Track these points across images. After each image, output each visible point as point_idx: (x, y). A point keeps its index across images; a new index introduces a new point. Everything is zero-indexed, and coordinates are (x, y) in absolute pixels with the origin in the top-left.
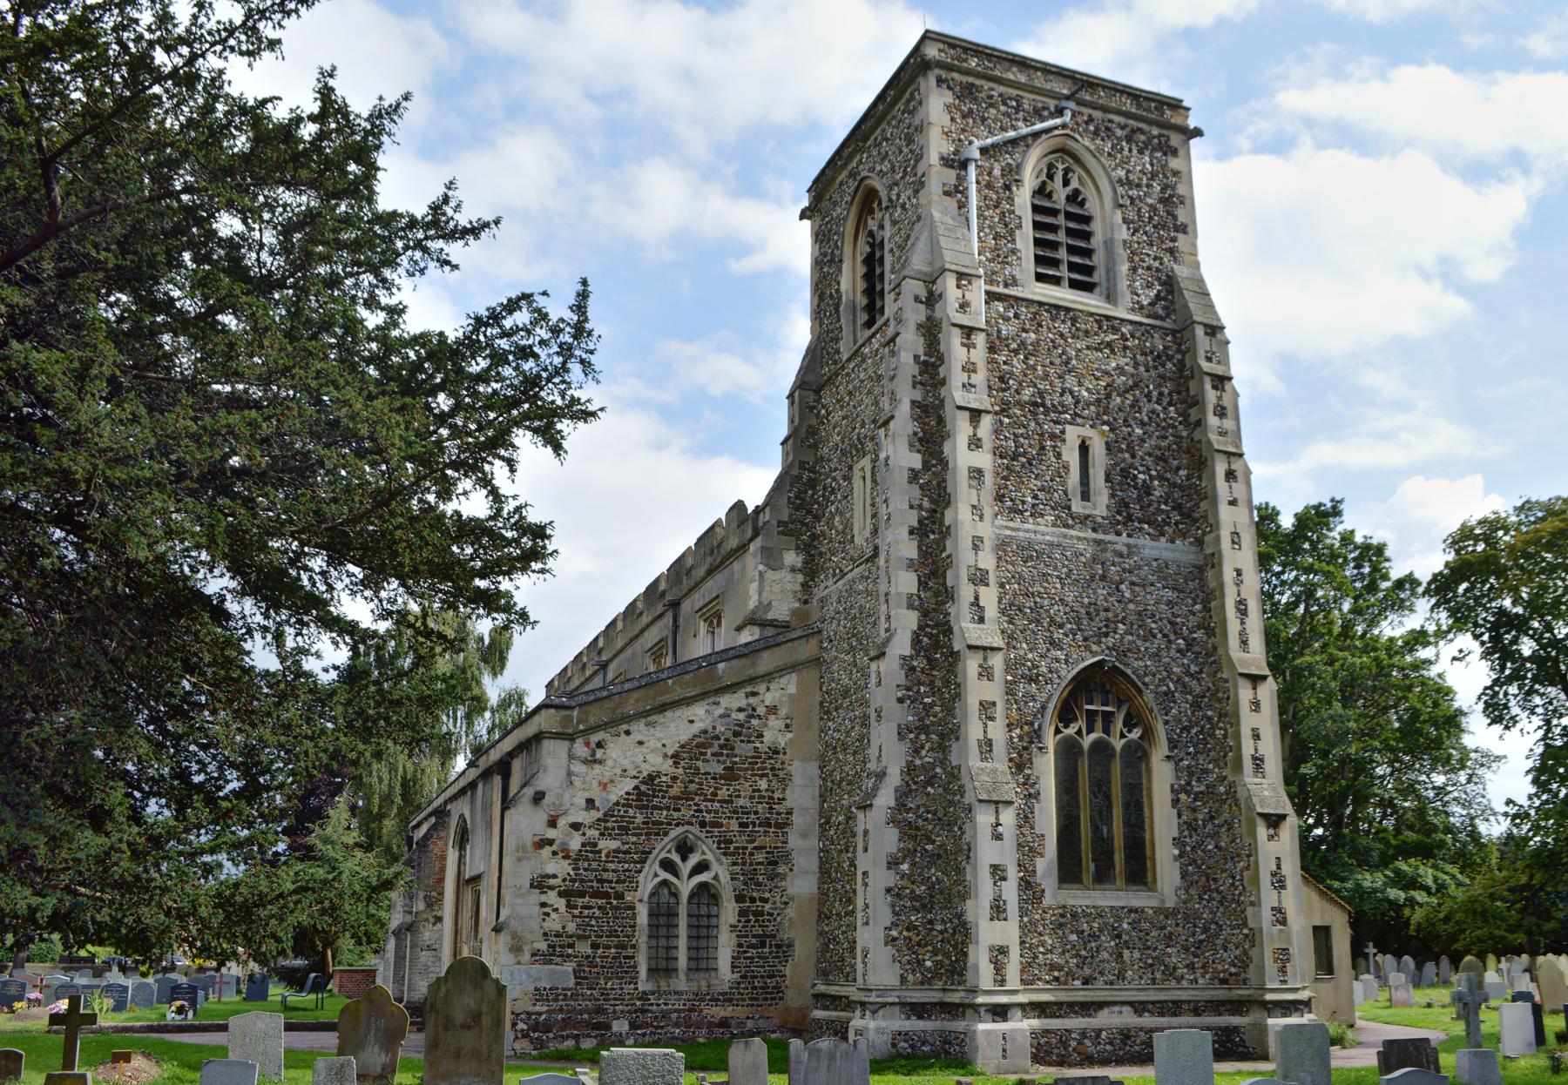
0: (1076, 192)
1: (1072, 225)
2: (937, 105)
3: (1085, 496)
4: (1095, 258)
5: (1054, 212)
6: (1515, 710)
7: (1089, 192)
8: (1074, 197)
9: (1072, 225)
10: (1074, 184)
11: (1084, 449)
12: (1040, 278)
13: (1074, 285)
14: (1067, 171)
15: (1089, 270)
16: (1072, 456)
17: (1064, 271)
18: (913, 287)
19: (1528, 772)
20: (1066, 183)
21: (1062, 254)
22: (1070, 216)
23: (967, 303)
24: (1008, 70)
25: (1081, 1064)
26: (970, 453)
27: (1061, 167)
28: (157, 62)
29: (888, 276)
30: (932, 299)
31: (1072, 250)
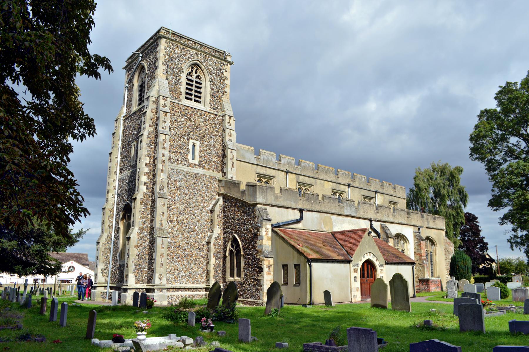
0: (199, 76)
1: (196, 85)
2: (163, 44)
3: (193, 159)
4: (202, 86)
5: (192, 81)
6: (456, 171)
7: (202, 76)
8: (198, 77)
9: (196, 85)
10: (198, 74)
11: (194, 146)
12: (187, 98)
13: (195, 101)
14: (197, 69)
15: (200, 97)
16: (191, 147)
17: (193, 97)
18: (152, 99)
19: (500, 87)
20: (196, 73)
21: (193, 92)
22: (196, 82)
23: (166, 105)
24: (217, 258)
25: (116, 215)
26: (163, 152)
27: (195, 68)
28: (54, 95)
29: (146, 86)
30: (157, 102)
31: (196, 91)
